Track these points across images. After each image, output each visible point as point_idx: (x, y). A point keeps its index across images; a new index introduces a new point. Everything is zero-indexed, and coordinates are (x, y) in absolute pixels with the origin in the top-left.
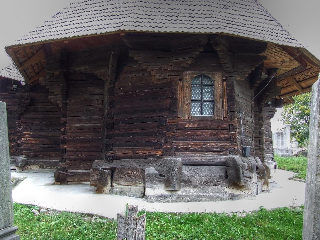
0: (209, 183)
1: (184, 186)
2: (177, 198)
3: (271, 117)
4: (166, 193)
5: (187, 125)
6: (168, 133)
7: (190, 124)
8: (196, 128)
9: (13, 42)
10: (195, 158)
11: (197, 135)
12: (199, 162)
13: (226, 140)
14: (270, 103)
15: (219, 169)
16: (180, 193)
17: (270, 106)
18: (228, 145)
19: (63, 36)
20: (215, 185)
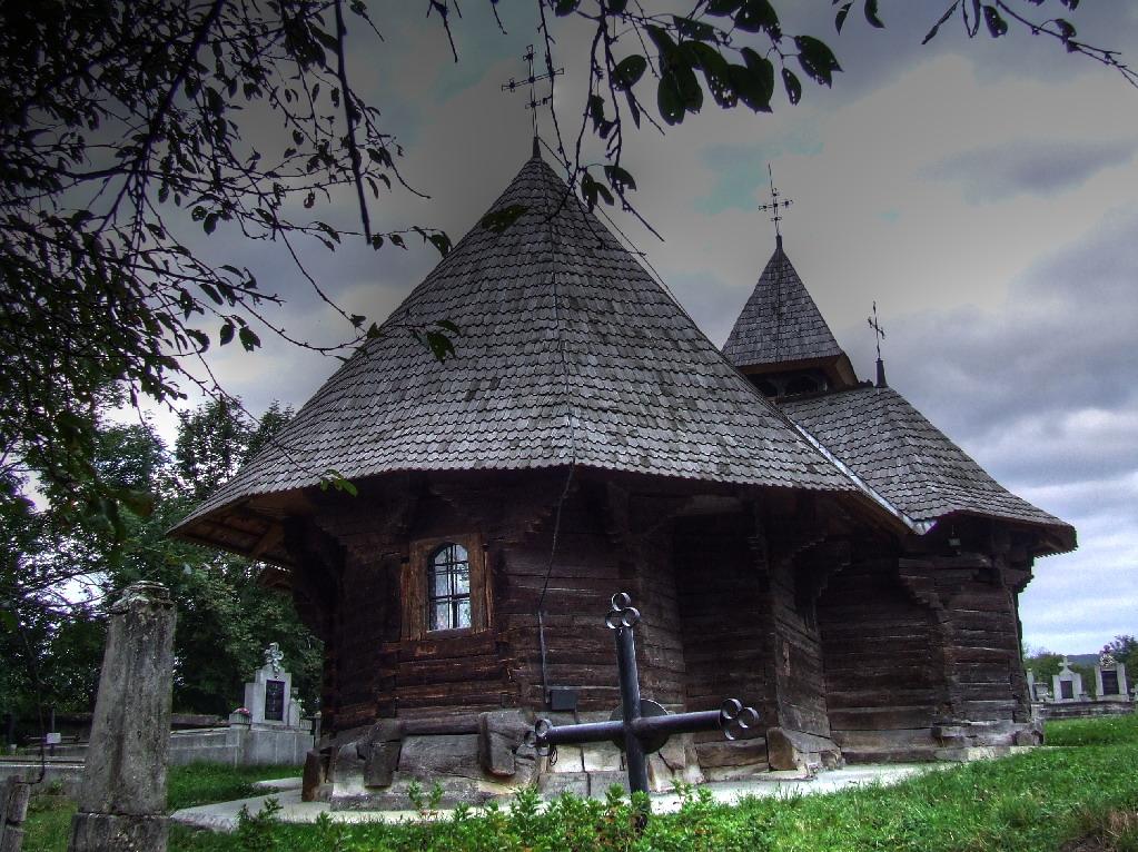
0: (445, 770)
1: (400, 778)
2: (379, 802)
3: (1020, 587)
4: (364, 792)
5: (419, 652)
6: (803, 647)
7: (422, 649)
8: (433, 657)
9: (767, 114)
10: (431, 720)
11: (436, 670)
12: (440, 728)
13: (491, 676)
14: (955, 542)
15: (564, 756)
16: (389, 792)
17: (959, 553)
18: (498, 689)
19: (385, 468)
20: (456, 775)
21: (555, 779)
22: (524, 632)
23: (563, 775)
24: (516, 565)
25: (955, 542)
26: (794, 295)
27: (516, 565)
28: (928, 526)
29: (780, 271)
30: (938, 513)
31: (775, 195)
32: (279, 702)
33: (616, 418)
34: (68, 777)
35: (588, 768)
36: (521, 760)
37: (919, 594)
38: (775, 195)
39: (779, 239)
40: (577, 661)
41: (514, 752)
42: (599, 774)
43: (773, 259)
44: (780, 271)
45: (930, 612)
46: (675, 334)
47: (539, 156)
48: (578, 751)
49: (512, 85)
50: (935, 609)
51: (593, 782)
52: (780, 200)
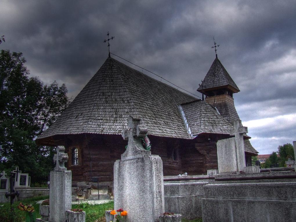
14: (209, 139)
21: (91, 196)
22: (87, 166)
23: (93, 195)
24: (86, 152)
25: (209, 139)
26: (107, 100)
27: (86, 152)
28: (195, 137)
29: (217, 64)
30: (198, 133)
31: (215, 44)
32: (21, 183)
33: (101, 121)
34: (43, 192)
35: (100, 194)
36: (83, 192)
37: (200, 152)
38: (215, 44)
39: (216, 55)
40: (99, 171)
41: (83, 191)
42: (101, 195)
43: (215, 61)
44: (217, 64)
45: (203, 155)
46: (124, 99)
47: (110, 57)
48: (98, 190)
49: (112, 38)
50: (205, 155)
51: (100, 196)
52: (216, 45)
